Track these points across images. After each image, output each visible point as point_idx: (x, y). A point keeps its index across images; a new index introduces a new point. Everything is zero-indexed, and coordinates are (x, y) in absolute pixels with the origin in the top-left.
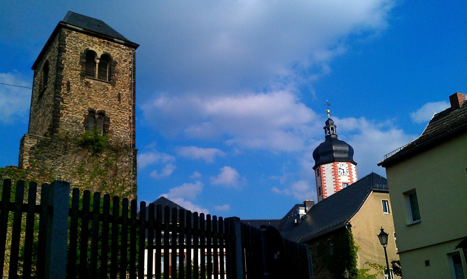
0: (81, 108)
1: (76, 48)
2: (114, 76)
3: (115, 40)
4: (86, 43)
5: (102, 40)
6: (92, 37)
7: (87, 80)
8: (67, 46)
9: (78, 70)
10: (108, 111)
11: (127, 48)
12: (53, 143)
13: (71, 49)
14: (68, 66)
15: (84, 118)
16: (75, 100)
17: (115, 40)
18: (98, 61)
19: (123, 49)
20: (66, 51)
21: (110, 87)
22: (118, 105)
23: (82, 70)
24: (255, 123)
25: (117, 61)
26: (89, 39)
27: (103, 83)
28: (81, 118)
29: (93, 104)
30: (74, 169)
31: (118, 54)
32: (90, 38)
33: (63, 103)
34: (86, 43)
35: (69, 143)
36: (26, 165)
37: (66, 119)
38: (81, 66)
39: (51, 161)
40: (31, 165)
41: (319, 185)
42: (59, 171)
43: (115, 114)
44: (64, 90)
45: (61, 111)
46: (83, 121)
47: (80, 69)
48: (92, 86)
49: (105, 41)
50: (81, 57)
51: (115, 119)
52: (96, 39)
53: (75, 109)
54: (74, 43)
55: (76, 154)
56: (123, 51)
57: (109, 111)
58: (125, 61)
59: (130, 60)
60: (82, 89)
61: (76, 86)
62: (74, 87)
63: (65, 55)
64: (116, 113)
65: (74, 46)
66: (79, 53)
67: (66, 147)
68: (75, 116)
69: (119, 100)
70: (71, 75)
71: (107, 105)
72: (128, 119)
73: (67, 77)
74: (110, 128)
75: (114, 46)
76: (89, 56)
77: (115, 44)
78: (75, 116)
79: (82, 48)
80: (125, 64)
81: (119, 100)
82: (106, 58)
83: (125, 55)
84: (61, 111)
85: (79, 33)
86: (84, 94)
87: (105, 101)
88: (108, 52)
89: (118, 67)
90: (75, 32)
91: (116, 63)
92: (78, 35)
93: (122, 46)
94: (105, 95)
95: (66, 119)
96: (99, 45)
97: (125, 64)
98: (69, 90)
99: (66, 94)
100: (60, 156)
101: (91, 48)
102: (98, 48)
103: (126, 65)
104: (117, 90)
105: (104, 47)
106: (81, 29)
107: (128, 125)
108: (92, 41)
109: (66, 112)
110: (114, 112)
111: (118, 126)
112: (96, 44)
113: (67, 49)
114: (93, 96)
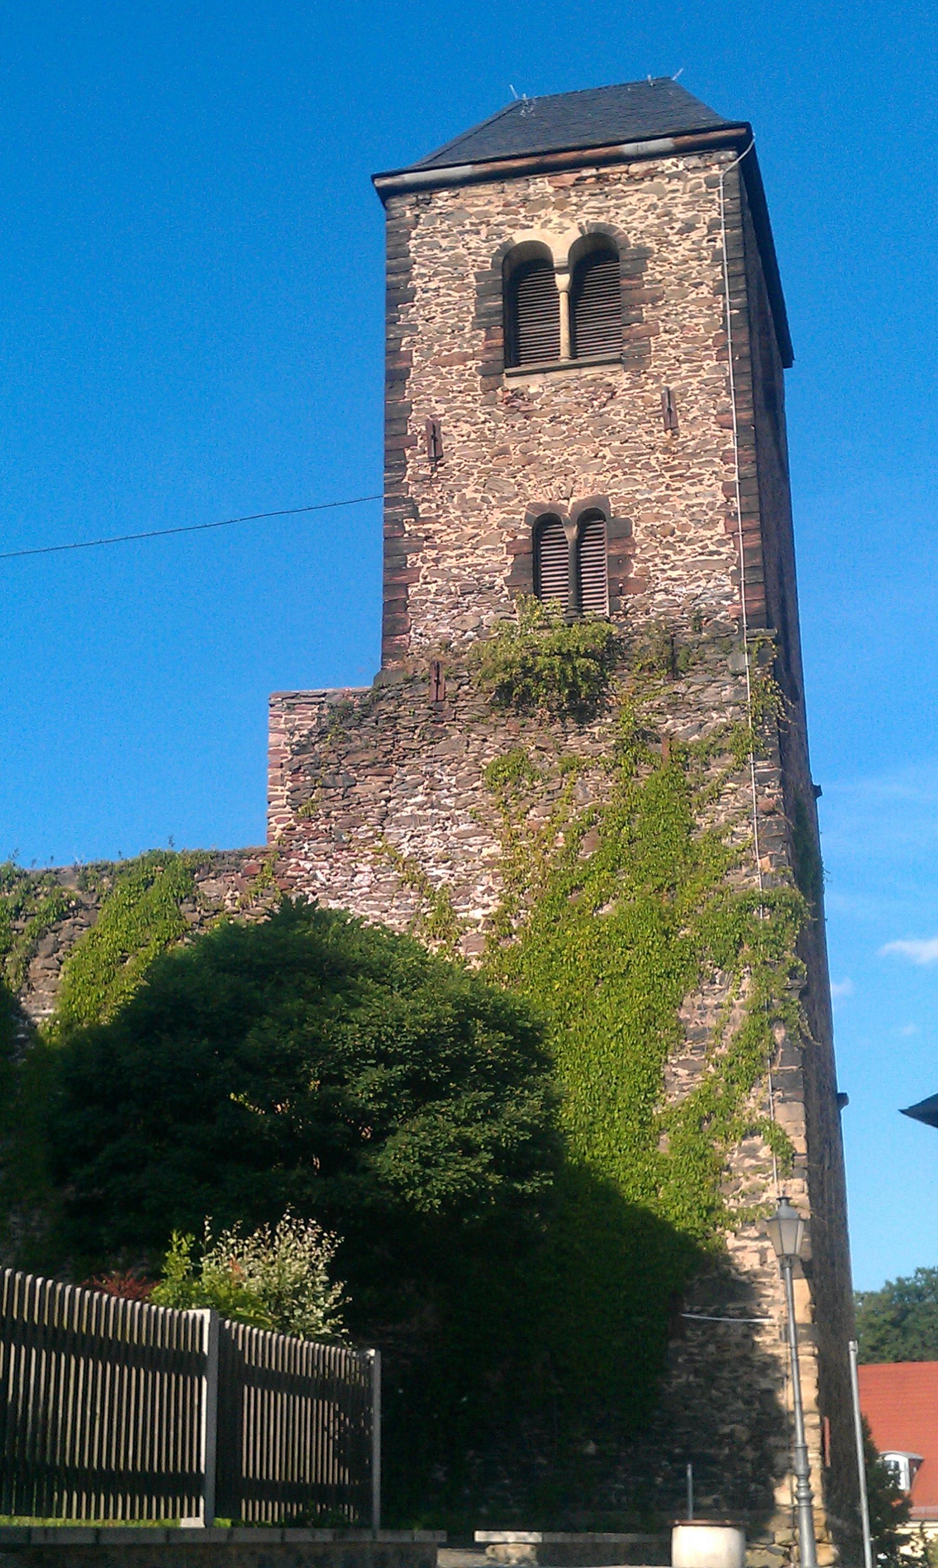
0: (497, 516)
1: (456, 262)
2: (640, 320)
3: (628, 148)
4: (500, 218)
5: (569, 178)
6: (522, 185)
7: (513, 384)
8: (416, 269)
9: (473, 357)
10: (619, 493)
11: (694, 161)
12: (383, 705)
13: (436, 274)
14: (426, 356)
15: (511, 560)
16: (469, 493)
17: (628, 148)
18: (562, 281)
19: (671, 177)
20: (414, 291)
21: (621, 379)
22: (666, 450)
23: (488, 349)
24: (402, 580)
25: (651, 244)
26: (510, 198)
27: (585, 371)
28: (498, 563)
29: (549, 482)
30: (478, 794)
31: (654, 206)
32: (513, 190)
33: (418, 520)
34: (500, 218)
35: (450, 687)
36: (279, 821)
37: (433, 588)
38: (483, 334)
39: (379, 781)
40: (298, 820)
41: (763, 1260)
42: (413, 816)
43: (652, 496)
44: (417, 463)
45: (411, 558)
46: (507, 573)
47: (480, 346)
48: (536, 405)
49: (586, 172)
50: (482, 294)
51: (658, 517)
52: (543, 186)
53: (469, 530)
54: (444, 243)
55: (480, 728)
56: (676, 184)
57: (623, 491)
58: (689, 227)
59: (714, 214)
60: (492, 431)
61: (465, 428)
62: (456, 436)
63: (413, 313)
64: (661, 491)
65: (444, 257)
66: (472, 278)
67: (436, 711)
68: (470, 560)
69: (672, 427)
70: (443, 390)
71: (617, 463)
72: (721, 498)
73: (425, 405)
74: (636, 566)
75: (632, 179)
76: (522, 270)
77: (635, 168)
78: (470, 560)
79: (479, 252)
80: (687, 244)
81: (672, 427)
82: (599, 253)
83: (686, 198)
84: (411, 558)
85: (462, 191)
86: (504, 452)
87: (606, 451)
88: (602, 219)
89: (653, 271)
90: (445, 194)
91: (643, 254)
92: (458, 201)
93: (668, 162)
94: (603, 427)
95: (433, 588)
96: (560, 206)
97: (687, 244)
98: (436, 459)
99: (426, 477)
100: (417, 752)
101: (520, 237)
102: (556, 220)
103: (697, 248)
104: (657, 378)
105: (579, 206)
106: (467, 170)
107: (721, 528)
108: (525, 201)
109: (433, 554)
110: (652, 488)
111: (670, 546)
112: (544, 205)
113: (418, 283)
114: (547, 446)
